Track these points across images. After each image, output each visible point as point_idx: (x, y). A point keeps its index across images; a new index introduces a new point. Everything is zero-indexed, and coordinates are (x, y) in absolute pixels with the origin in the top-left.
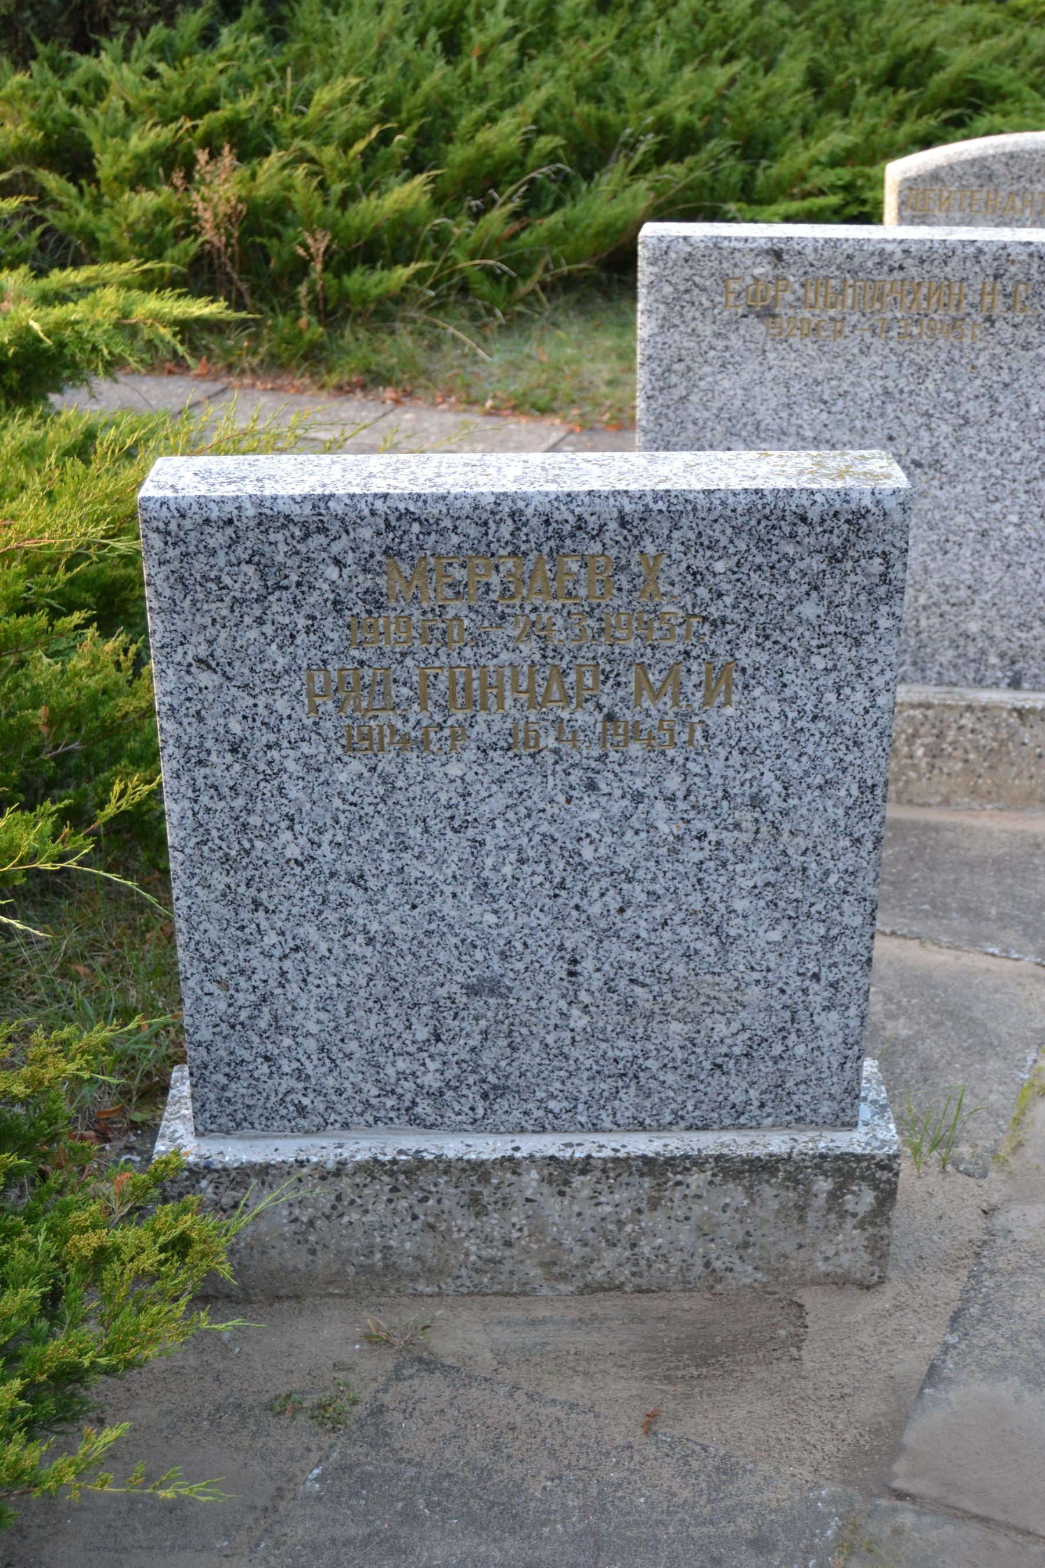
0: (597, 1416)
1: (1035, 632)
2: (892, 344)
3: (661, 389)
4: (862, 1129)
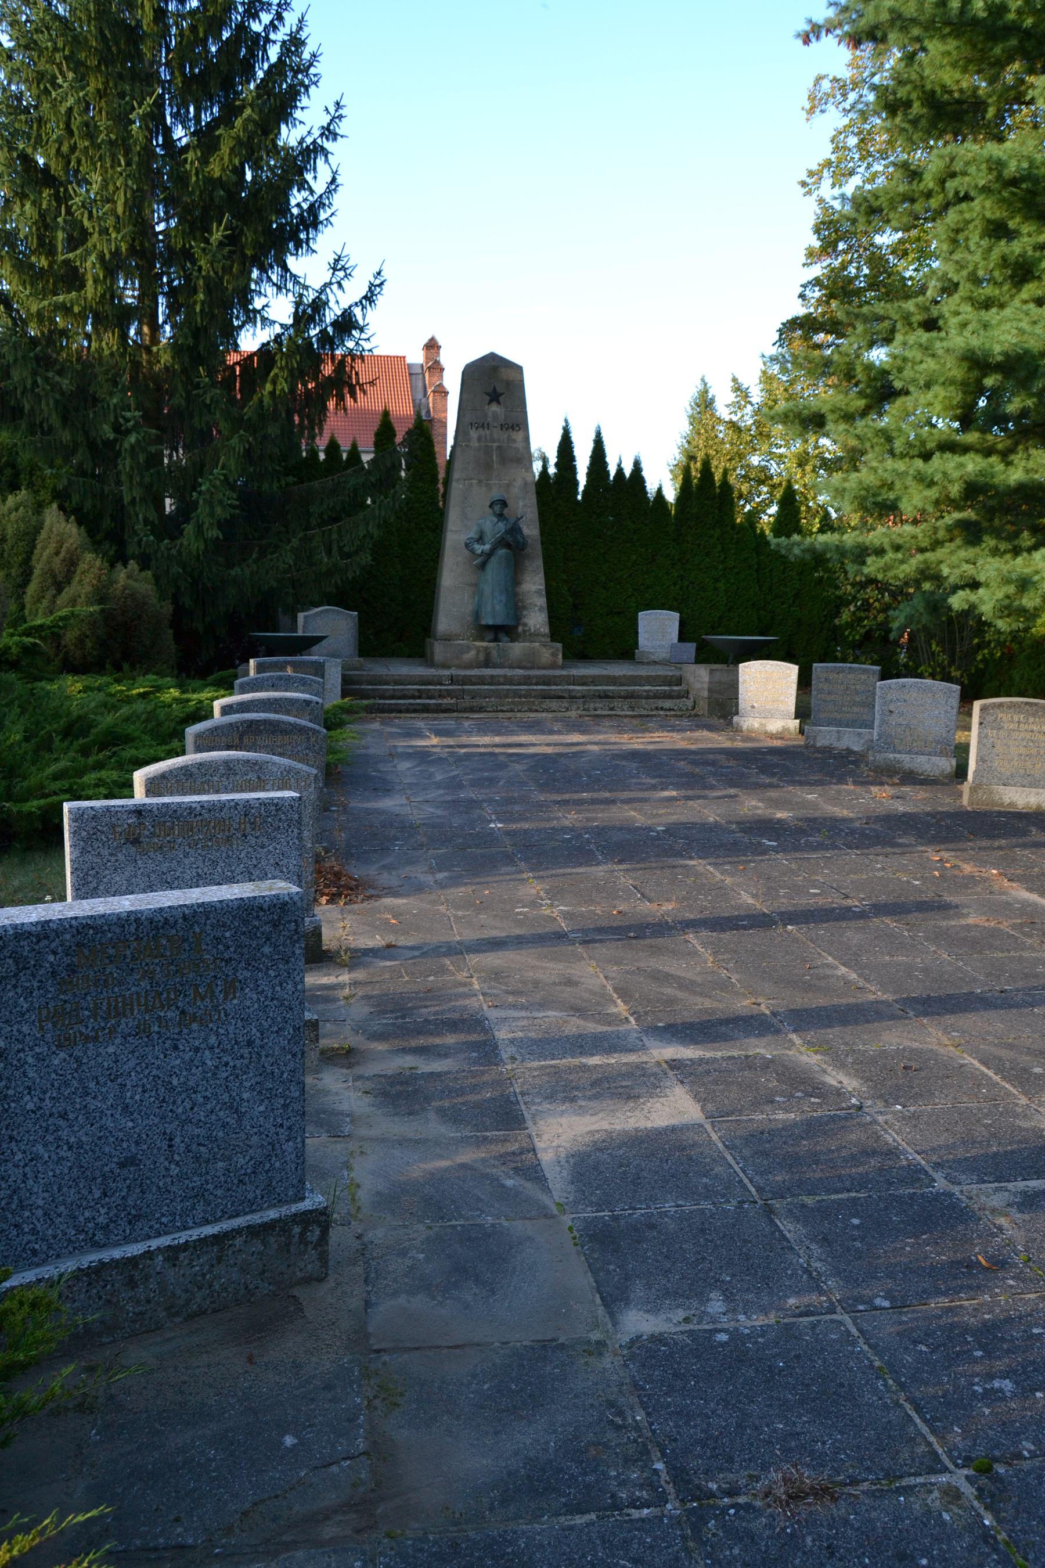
0: (224, 1365)
3: (83, 885)
4: (307, 1200)
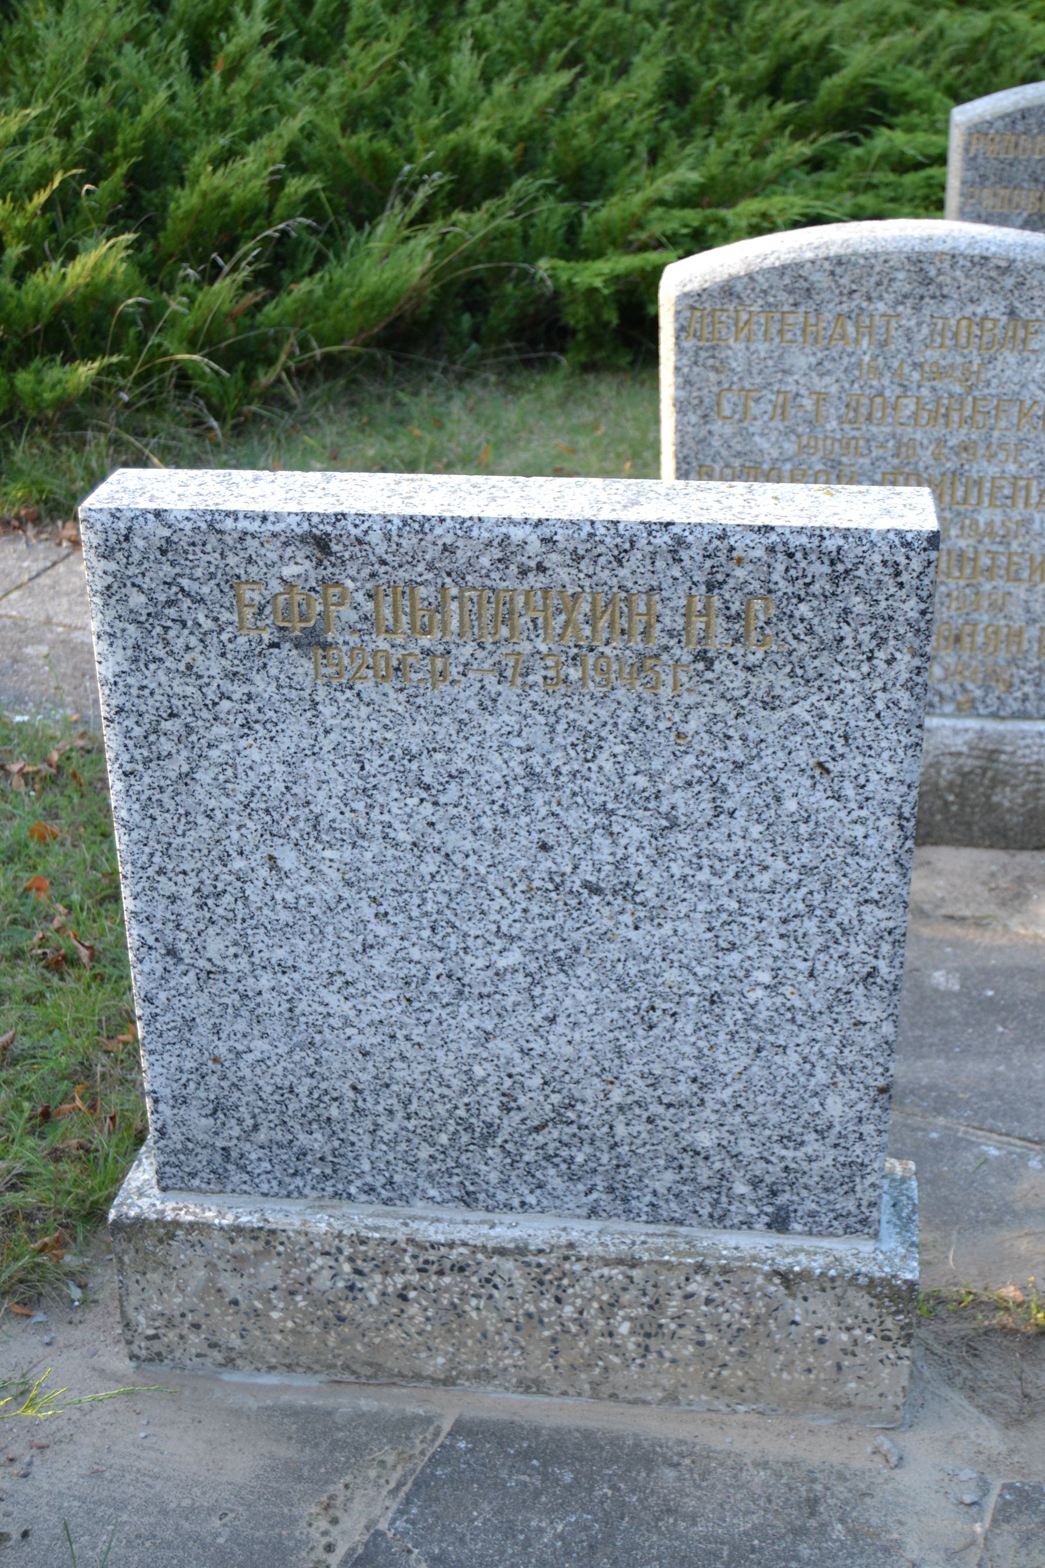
1: (808, 1149)
2: (534, 696)
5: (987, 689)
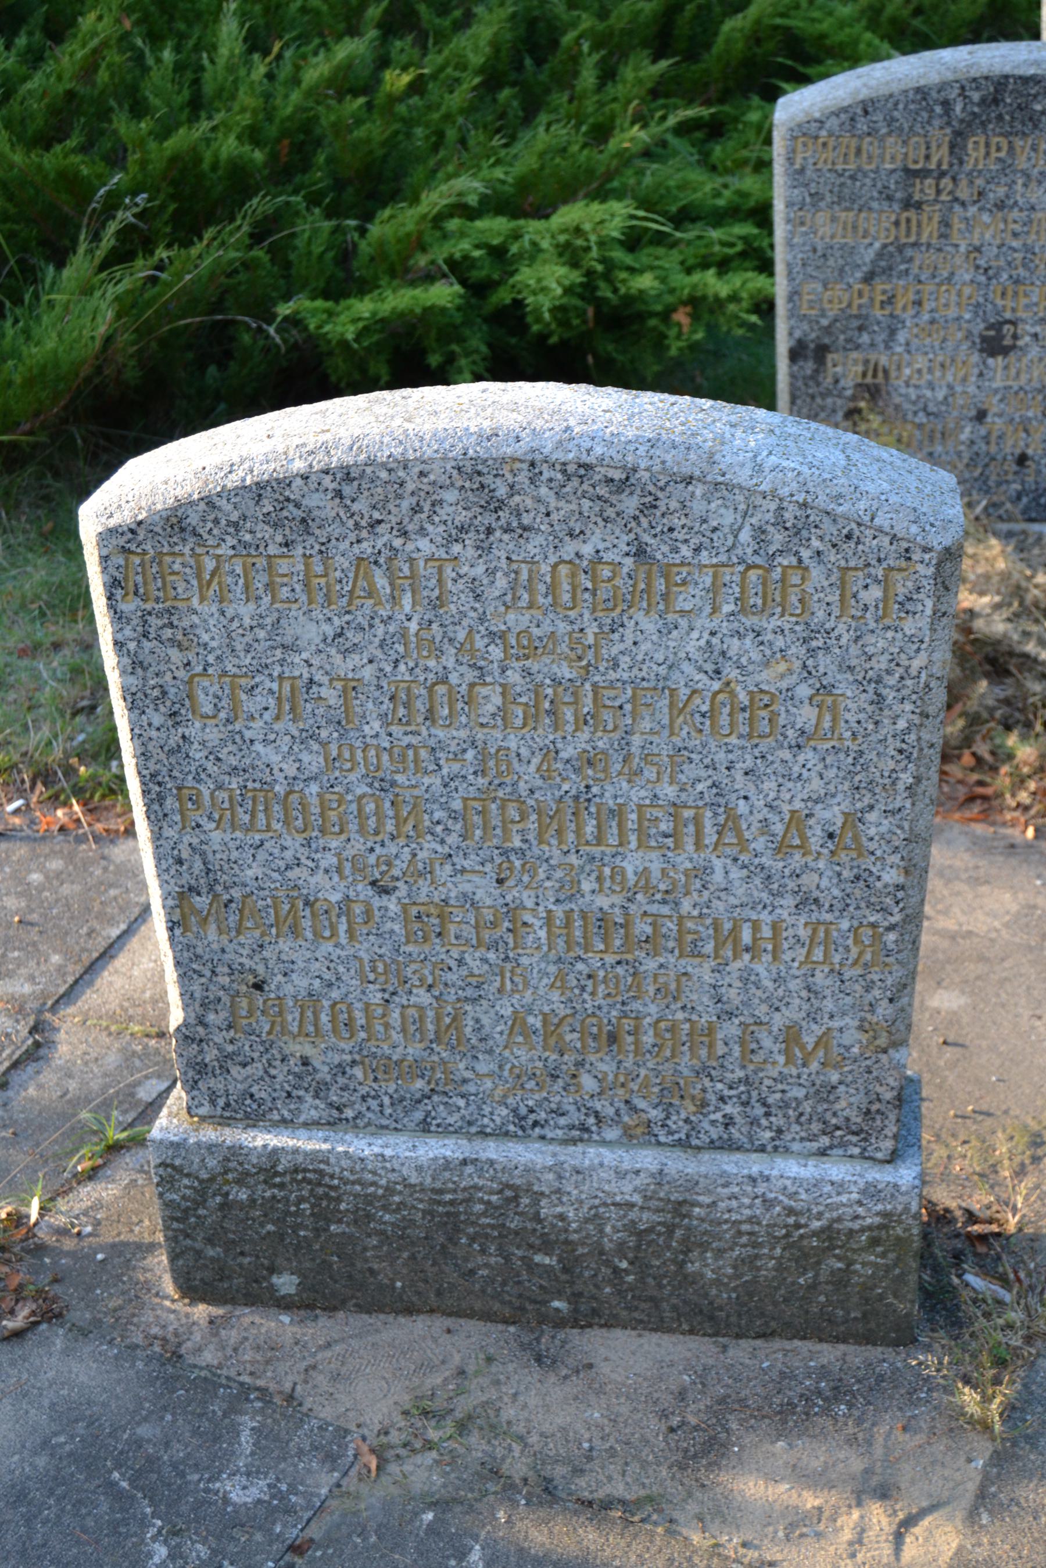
5: (668, 1110)
